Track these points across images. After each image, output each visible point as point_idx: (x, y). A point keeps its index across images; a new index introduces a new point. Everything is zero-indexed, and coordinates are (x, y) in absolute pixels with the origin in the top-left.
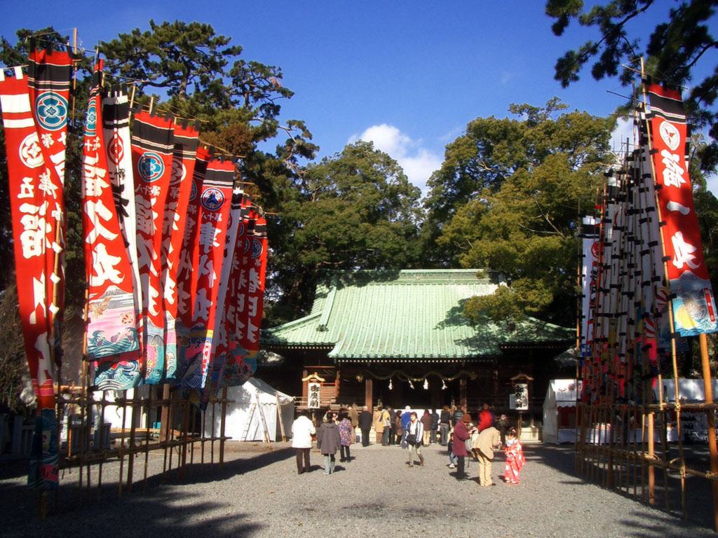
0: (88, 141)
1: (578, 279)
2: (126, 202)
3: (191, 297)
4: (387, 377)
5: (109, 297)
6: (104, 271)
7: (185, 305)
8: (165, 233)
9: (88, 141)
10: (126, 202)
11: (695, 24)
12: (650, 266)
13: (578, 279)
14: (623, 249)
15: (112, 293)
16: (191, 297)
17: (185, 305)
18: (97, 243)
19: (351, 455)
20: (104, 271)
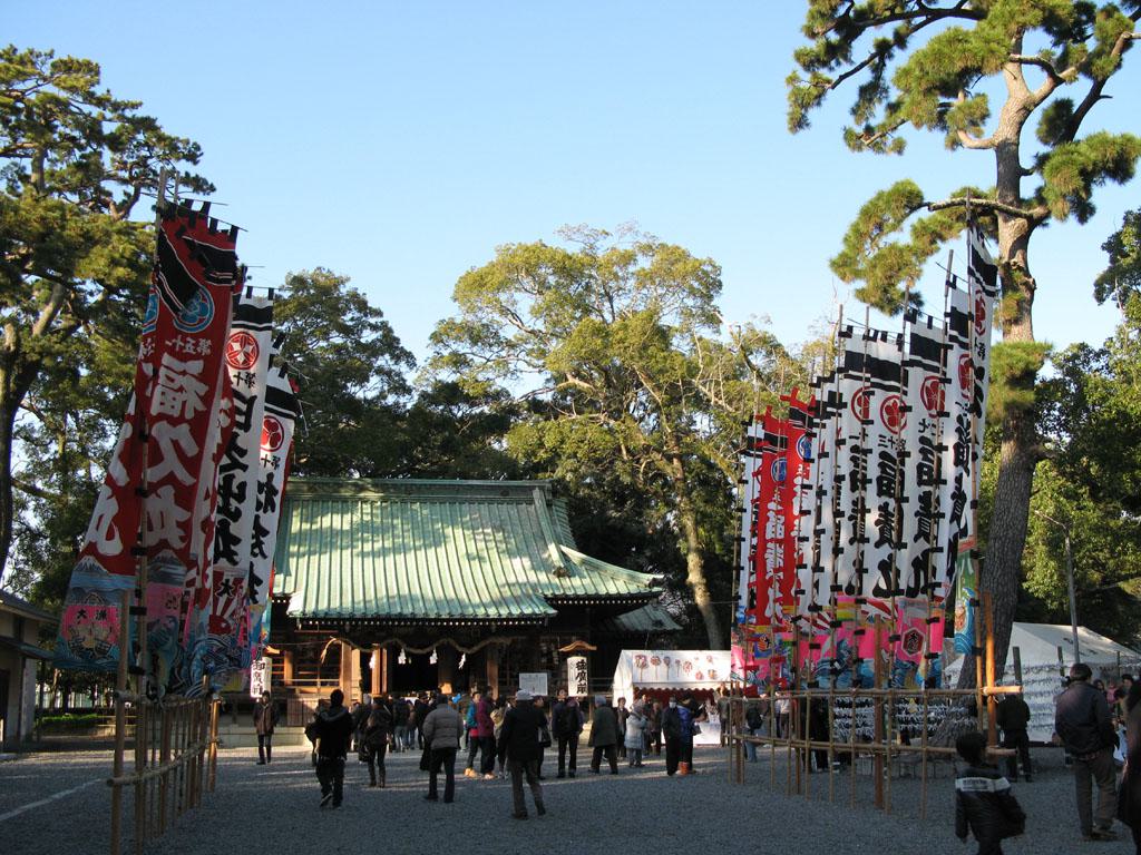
0: (180, 336)
1: (734, 572)
2: (237, 541)
3: (190, 519)
4: (428, 650)
5: (159, 564)
6: (163, 526)
7: (182, 534)
8: (257, 596)
9: (180, 336)
10: (237, 541)
11: (558, 615)
12: (917, 525)
13: (734, 572)
14: (821, 486)
15: (164, 560)
16: (190, 519)
17: (182, 534)
18: (162, 483)
19: (865, 567)
20: (163, 526)
